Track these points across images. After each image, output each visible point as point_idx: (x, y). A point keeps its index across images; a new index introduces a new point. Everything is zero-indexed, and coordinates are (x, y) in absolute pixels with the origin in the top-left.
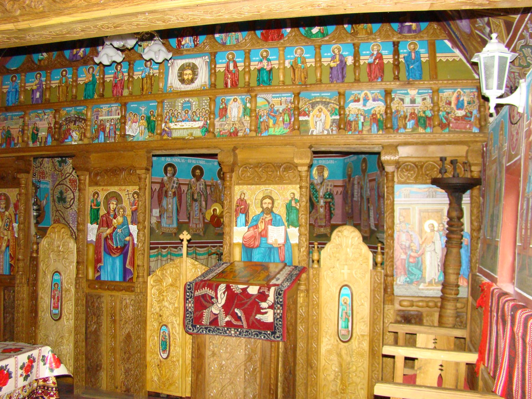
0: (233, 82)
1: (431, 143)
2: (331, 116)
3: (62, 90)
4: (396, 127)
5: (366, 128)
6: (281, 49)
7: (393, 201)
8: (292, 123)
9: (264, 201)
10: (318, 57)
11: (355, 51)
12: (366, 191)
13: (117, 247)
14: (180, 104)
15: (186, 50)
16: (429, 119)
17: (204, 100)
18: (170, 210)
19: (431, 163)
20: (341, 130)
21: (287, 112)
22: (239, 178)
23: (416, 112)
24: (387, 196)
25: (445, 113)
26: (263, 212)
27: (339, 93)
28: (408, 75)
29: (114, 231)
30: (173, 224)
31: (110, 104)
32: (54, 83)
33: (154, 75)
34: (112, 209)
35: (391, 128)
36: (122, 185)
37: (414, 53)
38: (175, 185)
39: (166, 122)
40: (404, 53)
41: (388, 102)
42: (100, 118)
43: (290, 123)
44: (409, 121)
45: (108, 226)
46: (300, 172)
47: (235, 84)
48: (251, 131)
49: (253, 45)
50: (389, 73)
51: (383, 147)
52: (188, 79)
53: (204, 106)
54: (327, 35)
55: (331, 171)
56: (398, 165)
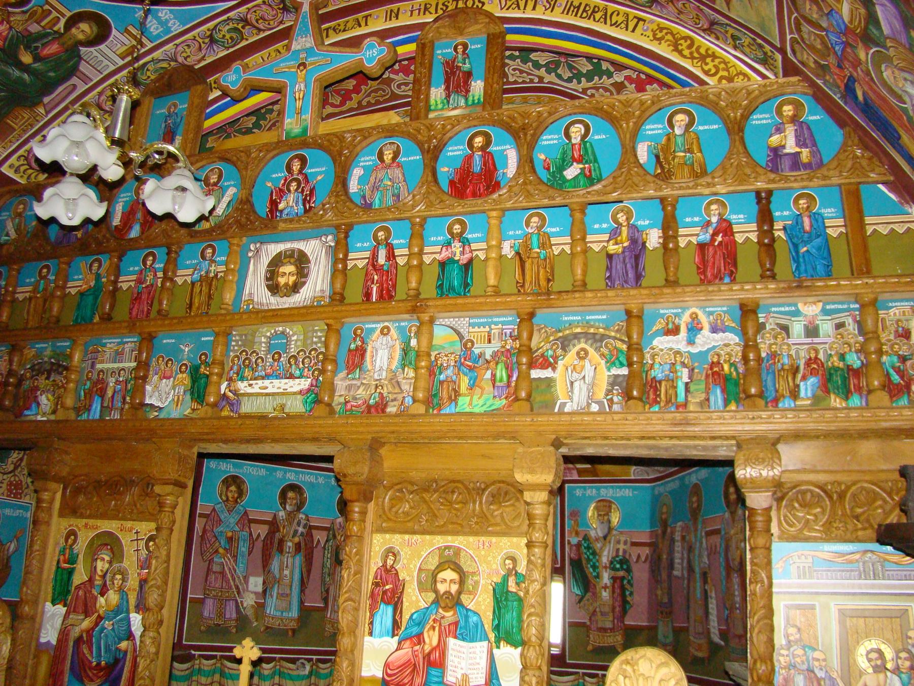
0: (383, 289)
1: (864, 435)
2: (609, 370)
3: (35, 305)
4: (771, 394)
5: (697, 398)
6: (494, 214)
7: (770, 585)
8: (513, 384)
9: (441, 575)
10: (579, 233)
11: (665, 217)
12: (700, 556)
13: (99, 664)
14: (263, 340)
15: (285, 221)
16: (857, 373)
17: (316, 331)
18: (287, 581)
19: (866, 485)
20: (631, 402)
21: (504, 358)
22: (382, 515)
23: (821, 356)
24: (752, 571)
25: (895, 359)
26: (436, 602)
27: (628, 313)
28: (797, 267)
29: (97, 624)
30: (289, 609)
31: (124, 336)
32: (23, 292)
33: (217, 275)
34: (100, 573)
35: (761, 395)
36: (124, 519)
37: (810, 217)
38: (301, 529)
39: (230, 380)
40: (784, 218)
41: (751, 332)
42: (99, 366)
43: (509, 382)
44: (804, 378)
45: (87, 614)
46: (528, 504)
47: (387, 295)
48: (414, 401)
49: (430, 205)
50: (748, 262)
51: (739, 446)
52: (286, 284)
53: (316, 343)
54: (599, 180)
55: (619, 515)
56: (780, 491)
